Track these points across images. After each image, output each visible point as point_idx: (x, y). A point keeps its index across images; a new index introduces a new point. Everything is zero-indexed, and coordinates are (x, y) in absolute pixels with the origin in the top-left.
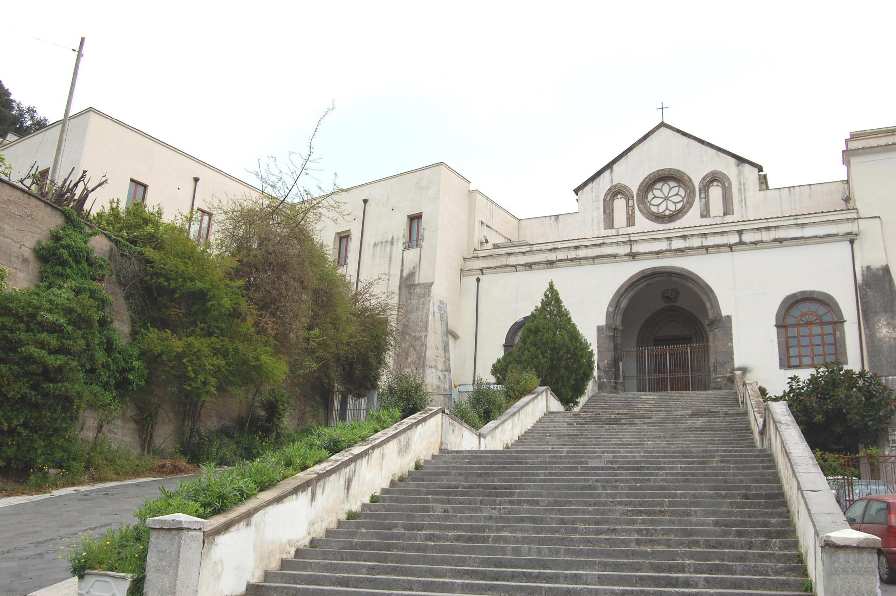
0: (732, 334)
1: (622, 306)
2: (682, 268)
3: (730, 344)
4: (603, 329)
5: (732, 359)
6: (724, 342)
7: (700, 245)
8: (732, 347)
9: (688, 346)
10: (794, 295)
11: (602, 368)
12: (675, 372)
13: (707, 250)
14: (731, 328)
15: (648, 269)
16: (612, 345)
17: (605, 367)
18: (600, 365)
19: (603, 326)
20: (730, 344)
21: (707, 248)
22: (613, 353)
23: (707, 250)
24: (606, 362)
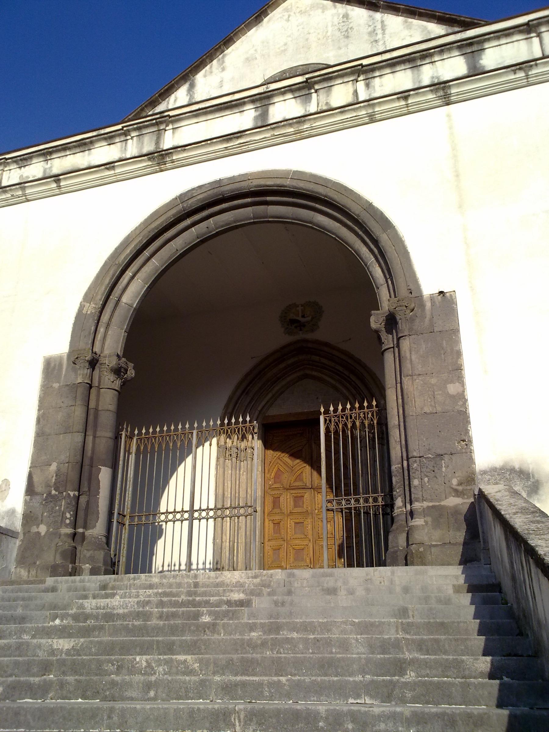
0: (459, 354)
1: (125, 299)
2: (295, 172)
3: (452, 389)
4: (61, 365)
5: (467, 441)
6: (433, 381)
7: (349, 99)
8: (461, 398)
9: (192, 427)
10: (80, 316)
11: (39, 488)
12: (347, 494)
13: (58, 181)
14: (456, 331)
15: (200, 187)
16: (79, 412)
17: (48, 486)
18: (36, 479)
19: (60, 358)
20: (452, 389)
21: (56, 178)
22: (79, 438)
23: (58, 181)
24: (54, 467)
